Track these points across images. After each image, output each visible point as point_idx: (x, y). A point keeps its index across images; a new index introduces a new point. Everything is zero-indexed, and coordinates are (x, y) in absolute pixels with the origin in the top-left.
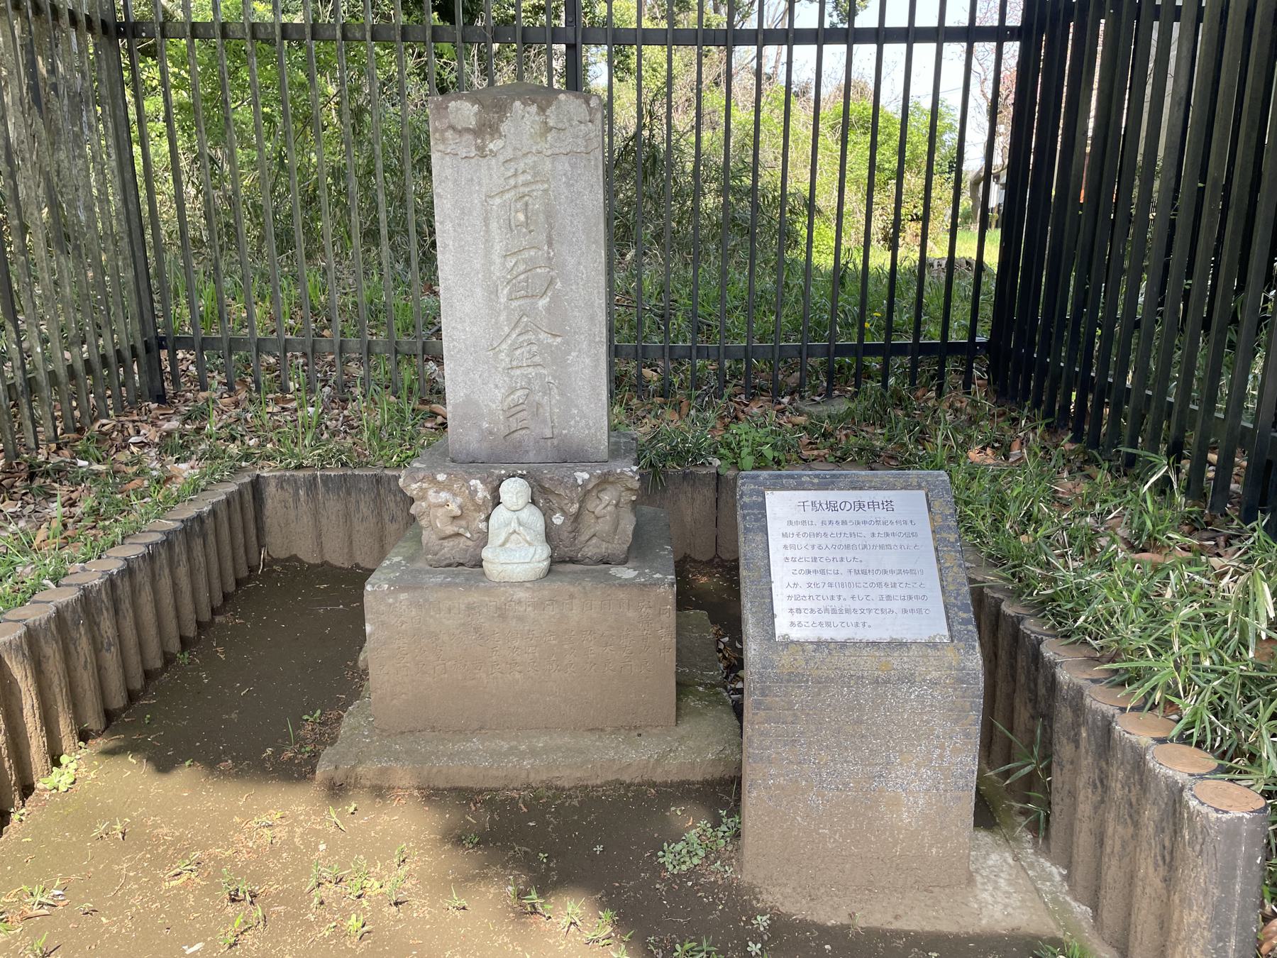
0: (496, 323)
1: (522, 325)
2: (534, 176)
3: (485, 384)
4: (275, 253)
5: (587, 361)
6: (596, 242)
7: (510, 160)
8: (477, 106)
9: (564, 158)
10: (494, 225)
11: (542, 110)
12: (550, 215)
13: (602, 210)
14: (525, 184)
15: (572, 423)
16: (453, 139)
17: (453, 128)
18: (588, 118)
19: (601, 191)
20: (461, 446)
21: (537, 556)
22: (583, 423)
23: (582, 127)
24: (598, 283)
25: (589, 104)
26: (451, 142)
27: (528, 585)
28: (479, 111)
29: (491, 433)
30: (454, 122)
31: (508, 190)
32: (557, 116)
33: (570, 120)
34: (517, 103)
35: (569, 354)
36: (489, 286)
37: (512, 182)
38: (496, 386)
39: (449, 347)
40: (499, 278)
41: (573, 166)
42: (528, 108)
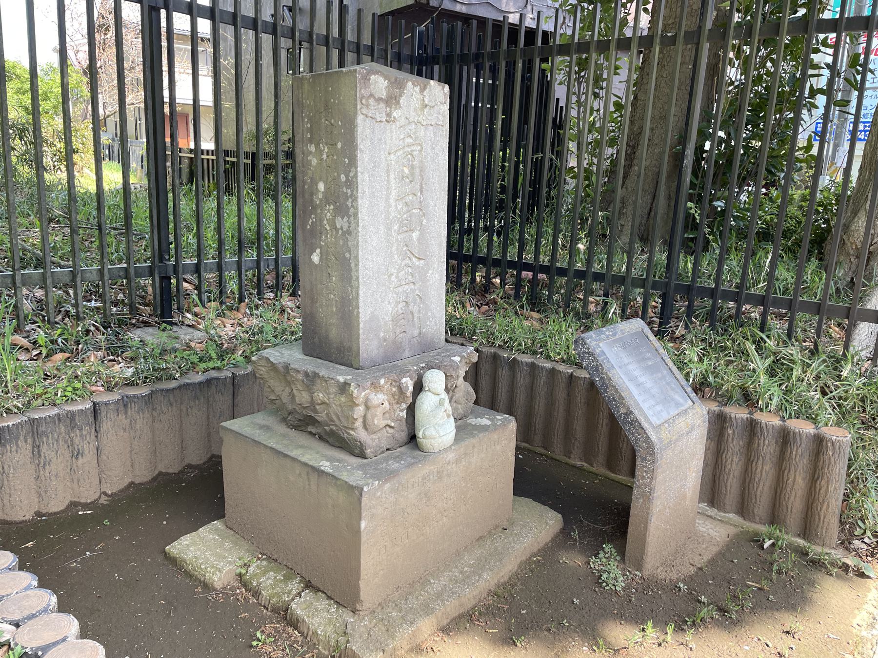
0: (391, 253)
10: (392, 176)
11: (422, 90)
36: (387, 224)
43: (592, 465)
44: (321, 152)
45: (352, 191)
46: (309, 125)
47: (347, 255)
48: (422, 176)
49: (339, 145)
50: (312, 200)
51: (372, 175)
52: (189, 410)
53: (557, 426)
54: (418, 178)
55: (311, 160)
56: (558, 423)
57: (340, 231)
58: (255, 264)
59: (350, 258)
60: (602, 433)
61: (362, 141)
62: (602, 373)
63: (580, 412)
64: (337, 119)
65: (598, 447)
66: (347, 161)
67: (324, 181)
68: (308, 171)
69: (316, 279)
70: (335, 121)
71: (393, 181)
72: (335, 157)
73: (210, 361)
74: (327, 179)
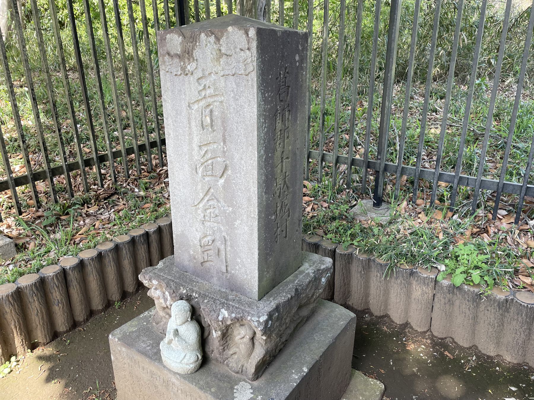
0: (196, 190)
1: (210, 194)
2: (215, 91)
3: (191, 227)
4: (453, 76)
5: (246, 228)
6: (252, 145)
7: (201, 78)
8: (181, 37)
9: (231, 78)
10: (193, 124)
11: (218, 39)
12: (224, 121)
13: (255, 121)
14: (211, 96)
15: (237, 267)
16: (169, 62)
17: (169, 54)
18: (247, 46)
19: (256, 106)
20: (180, 260)
21: (185, 360)
22: (243, 270)
23: (242, 53)
24: (253, 175)
25: (248, 35)
26: (168, 64)
27: (178, 376)
28: (183, 41)
29: (195, 258)
30: (170, 49)
31: (201, 99)
32: (227, 44)
33: (235, 48)
34: (203, 35)
35: (235, 221)
36: (191, 164)
37: (203, 94)
38: (197, 230)
39: (173, 199)
40: (197, 160)
41: (238, 85)
42: (209, 39)
48: (224, 127)
51: (175, 121)
54: (218, 123)
61: (165, 92)
71: (194, 129)
73: (277, 20)
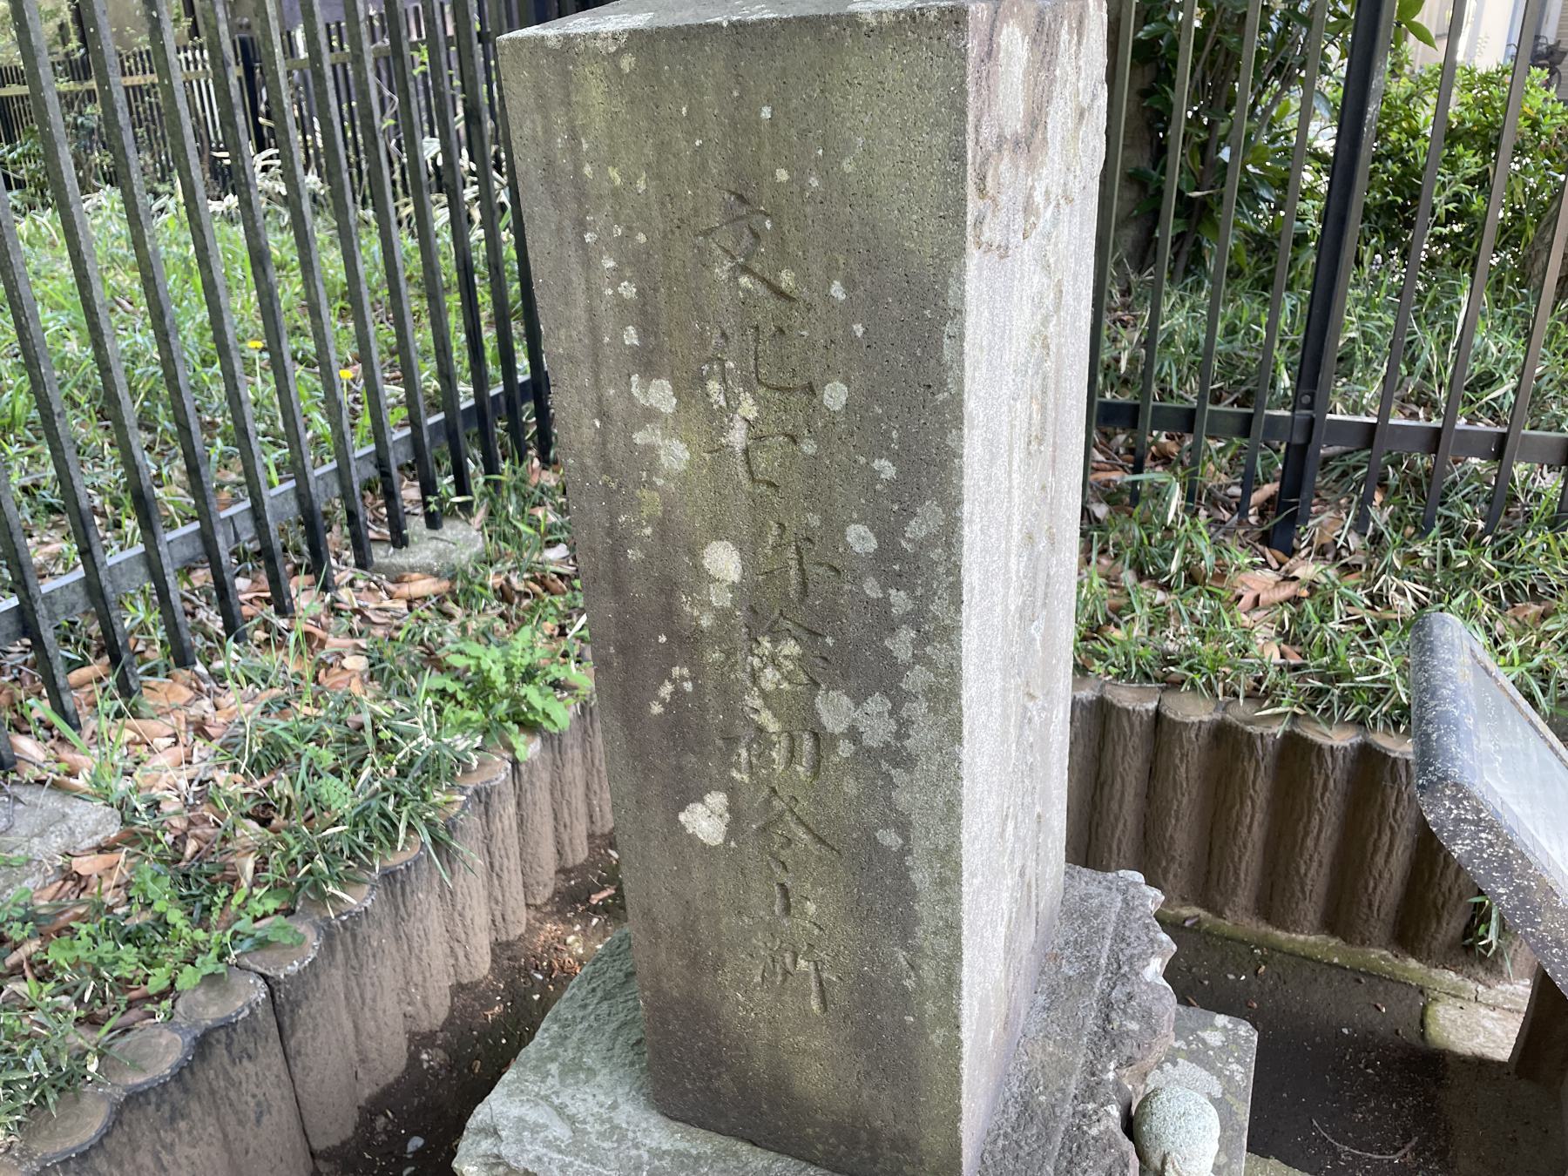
43: (1220, 914)
44: (717, 420)
45: (922, 603)
46: (628, 290)
47: (889, 839)
49: (835, 395)
50: (670, 613)
52: (165, 1156)
53: (1118, 833)
55: (650, 449)
56: (1120, 826)
57: (845, 749)
58: (198, 543)
59: (905, 851)
60: (1250, 845)
62: (1521, 876)
63: (1185, 800)
64: (817, 270)
65: (1237, 874)
66: (886, 468)
67: (739, 545)
68: (645, 493)
69: (711, 894)
70: (803, 277)
72: (809, 447)
74: (760, 535)
